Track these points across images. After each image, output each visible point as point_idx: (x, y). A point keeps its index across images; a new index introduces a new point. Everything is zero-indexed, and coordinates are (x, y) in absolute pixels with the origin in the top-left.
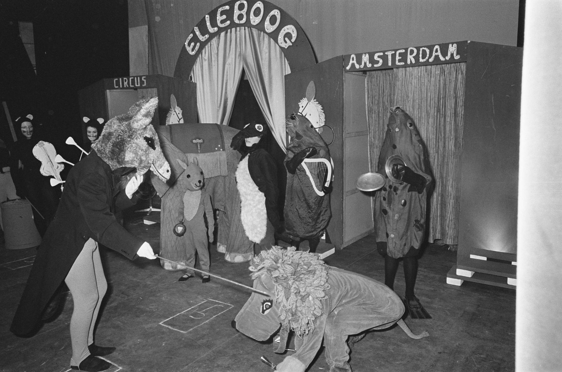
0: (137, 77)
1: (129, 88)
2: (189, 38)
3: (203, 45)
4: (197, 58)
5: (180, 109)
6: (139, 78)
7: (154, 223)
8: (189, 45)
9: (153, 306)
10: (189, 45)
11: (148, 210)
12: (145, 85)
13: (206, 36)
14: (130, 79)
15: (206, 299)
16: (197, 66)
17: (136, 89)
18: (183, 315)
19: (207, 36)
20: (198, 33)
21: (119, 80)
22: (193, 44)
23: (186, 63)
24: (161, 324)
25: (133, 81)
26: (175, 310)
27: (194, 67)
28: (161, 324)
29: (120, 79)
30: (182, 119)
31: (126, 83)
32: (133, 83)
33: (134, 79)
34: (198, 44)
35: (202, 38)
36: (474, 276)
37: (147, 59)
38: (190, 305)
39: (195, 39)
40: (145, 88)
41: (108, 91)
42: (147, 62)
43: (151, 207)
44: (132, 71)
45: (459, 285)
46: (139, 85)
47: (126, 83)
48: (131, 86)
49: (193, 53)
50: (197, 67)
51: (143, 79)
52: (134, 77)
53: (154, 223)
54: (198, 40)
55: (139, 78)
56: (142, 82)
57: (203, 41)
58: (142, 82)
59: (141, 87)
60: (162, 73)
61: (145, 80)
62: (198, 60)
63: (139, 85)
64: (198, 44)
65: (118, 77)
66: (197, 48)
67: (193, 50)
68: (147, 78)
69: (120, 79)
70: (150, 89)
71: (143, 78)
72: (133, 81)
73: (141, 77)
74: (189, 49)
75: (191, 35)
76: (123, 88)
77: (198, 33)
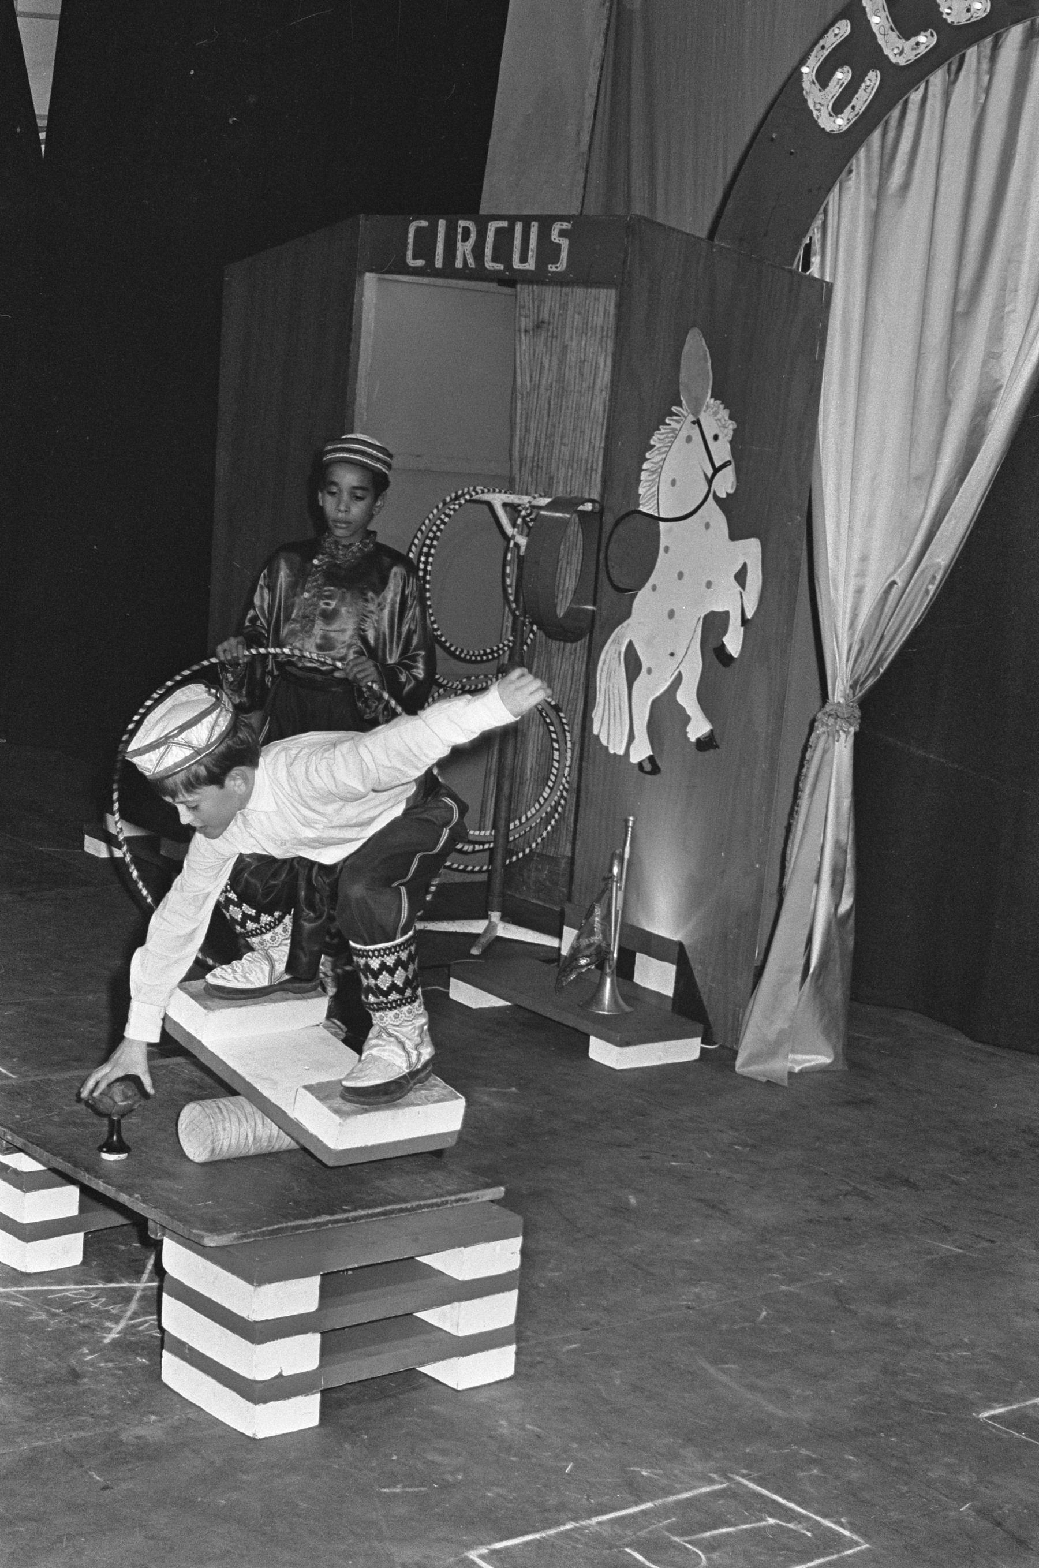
0: (527, 221)
1: (479, 274)
2: (831, 41)
3: (900, 82)
4: (854, 151)
5: (724, 414)
6: (535, 227)
7: (500, 1003)
8: (823, 78)
9: (443, 1452)
10: (823, 78)
11: (477, 927)
12: (562, 266)
13: (922, 39)
14: (493, 226)
15: (724, 1474)
16: (849, 194)
17: (510, 280)
18: (597, 1539)
19: (926, 40)
20: (878, 21)
21: (434, 227)
22: (842, 75)
23: (788, 173)
24: (473, 1555)
25: (504, 236)
26: (552, 1501)
27: (833, 197)
28: (473, 1555)
29: (442, 224)
30: (730, 471)
31: (464, 249)
32: (502, 253)
33: (511, 229)
34: (873, 79)
35: (899, 50)
36: (325, 1293)
37: (587, 124)
38: (638, 1491)
39: (861, 52)
40: (559, 281)
41: (369, 277)
42: (586, 138)
43: (495, 916)
44: (499, 188)
45: (315, 1421)
46: (531, 265)
47: (464, 249)
48: (489, 265)
49: (840, 123)
50: (849, 204)
51: (555, 237)
52: (512, 220)
53: (500, 1003)
54: (877, 59)
55: (535, 227)
56: (548, 252)
57: (902, 61)
58: (548, 252)
59: (538, 278)
60: (653, 207)
61: (565, 243)
62: (863, 163)
63: (531, 265)
64: (873, 79)
65: (432, 212)
66: (862, 99)
67: (838, 108)
68: (581, 228)
69: (442, 224)
70: (579, 292)
71: (557, 227)
72: (504, 236)
73: (546, 223)
74: (819, 101)
75: (843, 29)
76: (449, 271)
77: (878, 21)
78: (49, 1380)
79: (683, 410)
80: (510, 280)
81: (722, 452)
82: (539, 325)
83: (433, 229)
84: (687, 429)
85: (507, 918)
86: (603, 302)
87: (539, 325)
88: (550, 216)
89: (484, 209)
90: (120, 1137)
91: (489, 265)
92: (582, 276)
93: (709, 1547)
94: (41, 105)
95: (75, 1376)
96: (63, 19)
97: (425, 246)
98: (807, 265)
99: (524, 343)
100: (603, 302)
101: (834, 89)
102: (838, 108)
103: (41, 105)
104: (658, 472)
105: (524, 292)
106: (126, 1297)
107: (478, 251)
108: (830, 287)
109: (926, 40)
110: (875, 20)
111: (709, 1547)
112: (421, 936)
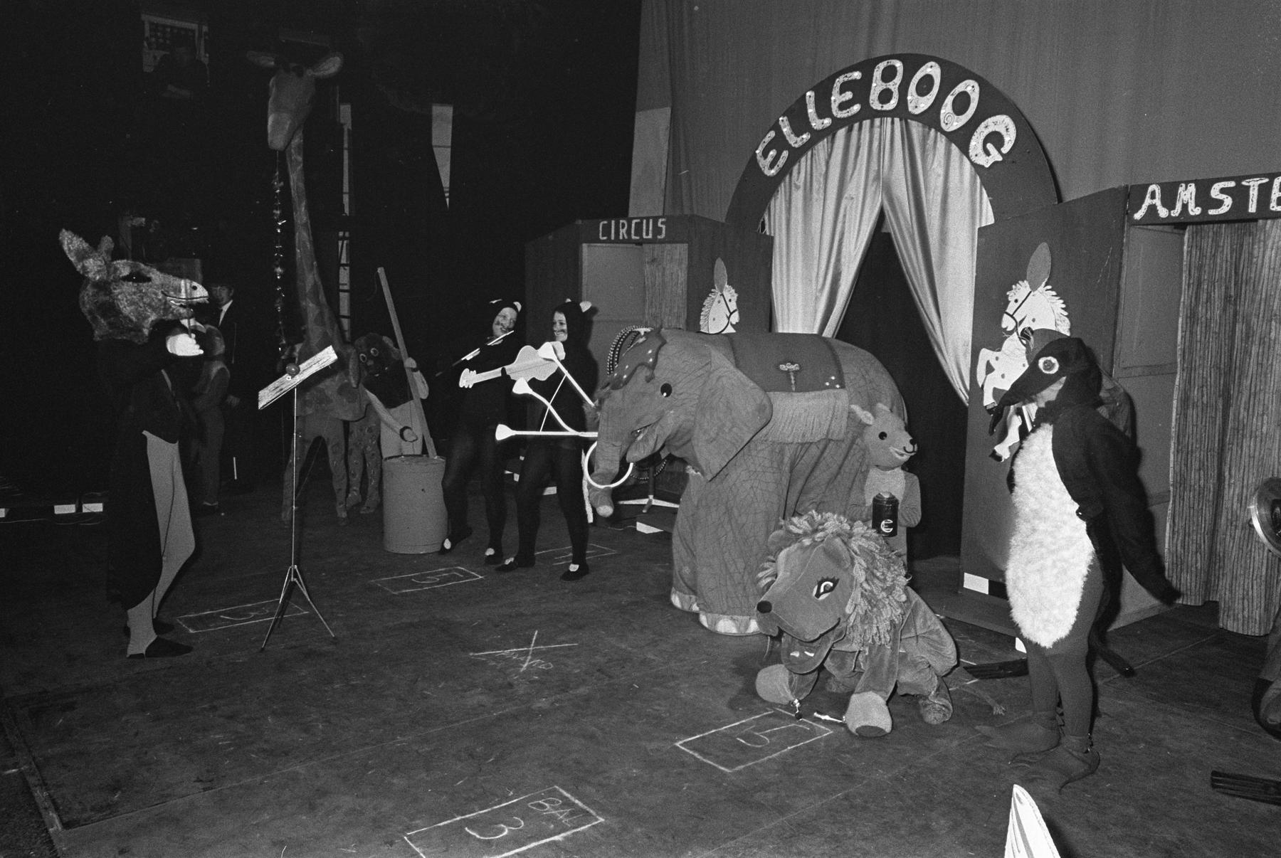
0: (648, 219)
1: (629, 241)
2: (767, 139)
3: (796, 155)
4: (779, 184)
8: (765, 154)
10: (765, 154)
11: (644, 501)
12: (663, 236)
13: (804, 136)
16: (778, 201)
17: (640, 243)
18: (724, 735)
19: (806, 137)
22: (773, 153)
23: (756, 193)
24: (678, 744)
25: (639, 226)
28: (678, 744)
31: (623, 231)
34: (785, 154)
35: (795, 141)
39: (780, 142)
40: (662, 242)
41: (584, 245)
43: (651, 497)
46: (650, 236)
47: (623, 231)
49: (773, 172)
52: (642, 219)
54: (789, 147)
56: (657, 231)
58: (657, 231)
59: (653, 241)
63: (650, 236)
64: (785, 154)
65: (609, 218)
66: (781, 162)
70: (668, 246)
72: (639, 226)
73: (656, 219)
74: (764, 164)
75: (772, 134)
76: (617, 241)
78: (501, 687)
79: (716, 290)
80: (640, 243)
81: (733, 306)
82: (654, 260)
83: (610, 225)
84: (718, 298)
85: (656, 497)
86: (681, 250)
87: (654, 260)
88: (1005, 99)
89: (630, 215)
90: (1027, 642)
91: (633, 237)
92: (671, 239)
93: (769, 736)
94: (446, 182)
95: (511, 685)
96: (452, 147)
97: (607, 231)
98: (763, 228)
99: (647, 268)
100: (681, 250)
101: (770, 159)
102: (771, 167)
103: (446, 182)
104: (707, 316)
105: (646, 246)
106: (527, 653)
107: (629, 232)
108: (772, 238)
109: (806, 137)
110: (785, 130)
111: (769, 736)
112: (677, 502)
